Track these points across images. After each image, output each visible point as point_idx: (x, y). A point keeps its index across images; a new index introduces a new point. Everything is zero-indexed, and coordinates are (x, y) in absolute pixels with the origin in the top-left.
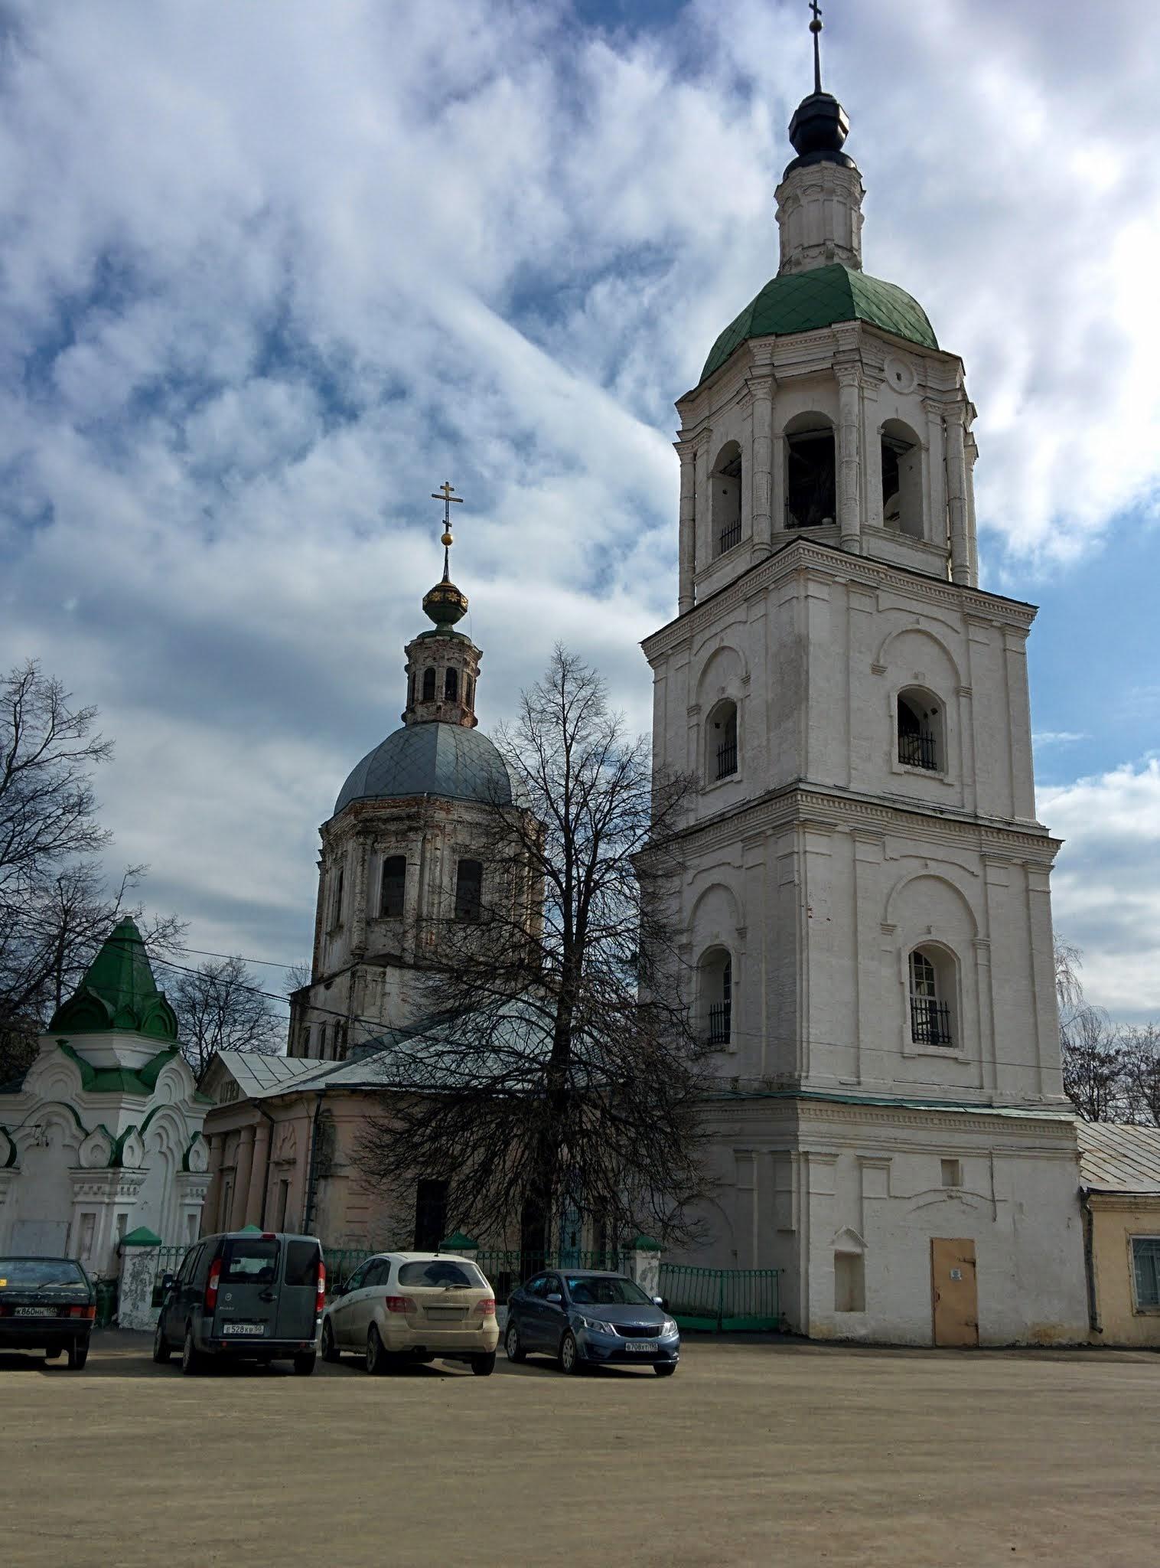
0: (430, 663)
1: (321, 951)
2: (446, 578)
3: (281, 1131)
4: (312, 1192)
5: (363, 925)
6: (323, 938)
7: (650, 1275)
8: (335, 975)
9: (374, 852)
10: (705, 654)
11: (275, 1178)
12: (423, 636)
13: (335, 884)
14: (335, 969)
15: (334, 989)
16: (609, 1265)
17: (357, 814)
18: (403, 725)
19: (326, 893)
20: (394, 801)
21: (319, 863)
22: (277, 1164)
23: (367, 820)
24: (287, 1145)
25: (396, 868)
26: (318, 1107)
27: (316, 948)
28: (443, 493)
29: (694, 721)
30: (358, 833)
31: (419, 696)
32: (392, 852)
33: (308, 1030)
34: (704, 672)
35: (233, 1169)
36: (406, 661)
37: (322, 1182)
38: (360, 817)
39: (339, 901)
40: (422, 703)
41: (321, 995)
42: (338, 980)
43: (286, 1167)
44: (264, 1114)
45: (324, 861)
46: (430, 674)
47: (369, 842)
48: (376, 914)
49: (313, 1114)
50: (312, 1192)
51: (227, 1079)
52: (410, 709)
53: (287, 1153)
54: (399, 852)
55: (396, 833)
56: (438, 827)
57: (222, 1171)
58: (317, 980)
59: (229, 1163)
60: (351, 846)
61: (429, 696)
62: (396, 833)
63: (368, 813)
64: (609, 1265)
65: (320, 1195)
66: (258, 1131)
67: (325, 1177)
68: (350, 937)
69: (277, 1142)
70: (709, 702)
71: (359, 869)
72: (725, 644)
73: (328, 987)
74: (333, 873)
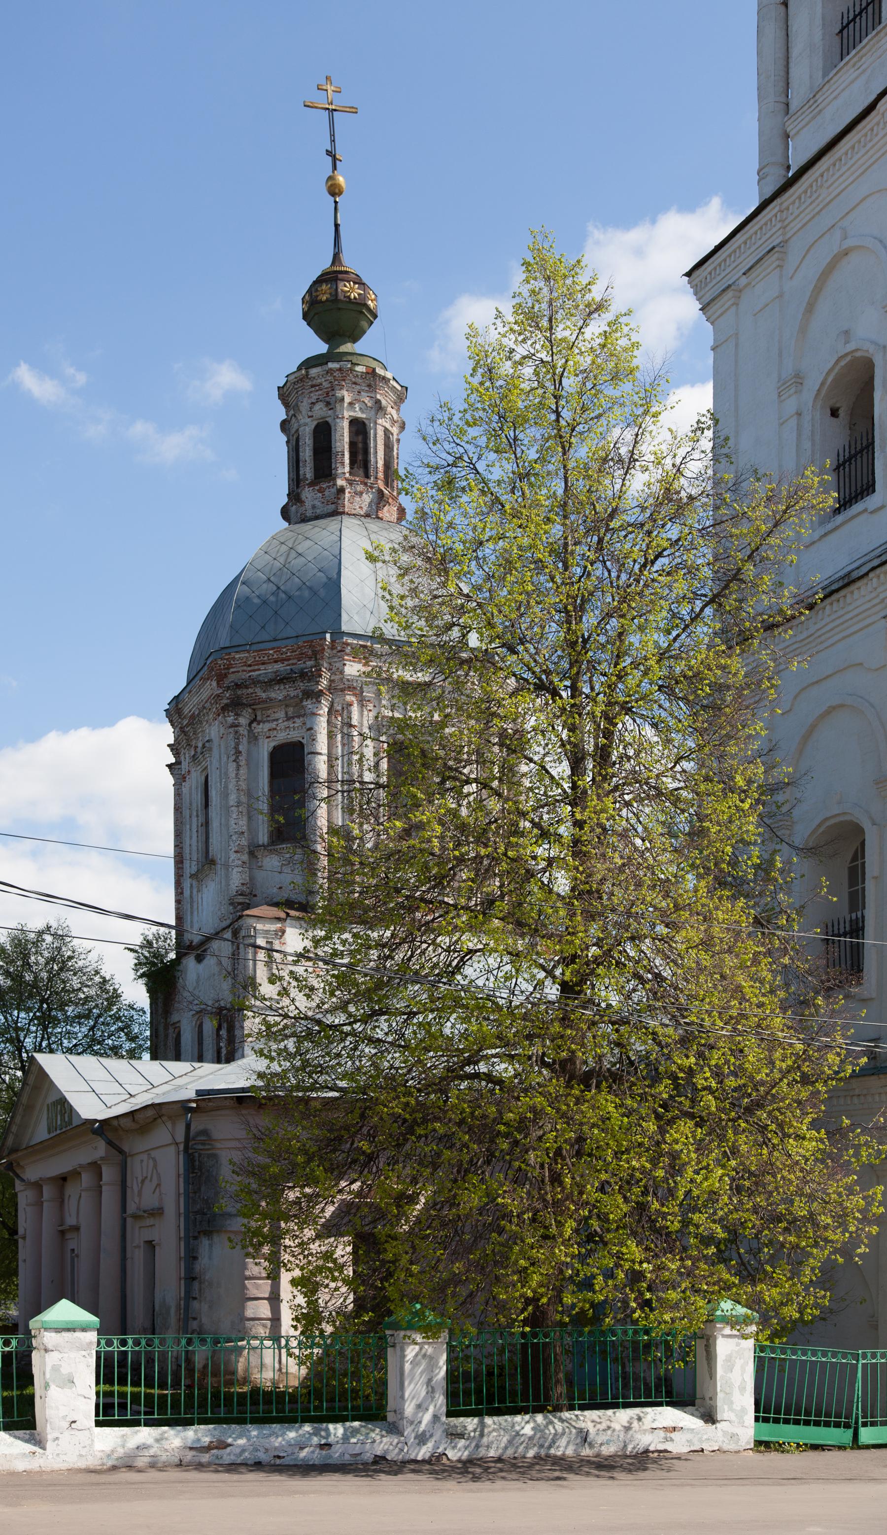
0: (320, 410)
1: (187, 906)
2: (336, 258)
3: (138, 1168)
4: (191, 1257)
5: (245, 858)
6: (187, 884)
7: (739, 1363)
8: (208, 939)
9: (253, 738)
10: (811, 270)
11: (138, 1235)
12: (310, 363)
13: (198, 798)
14: (209, 928)
15: (210, 961)
16: (848, 944)
17: (221, 678)
18: (286, 524)
19: (186, 813)
20: (278, 650)
21: (170, 766)
22: (136, 1217)
23: (238, 686)
24: (149, 1187)
25: (290, 763)
26: (188, 1127)
27: (178, 902)
28: (320, 100)
29: (791, 405)
30: (224, 709)
31: (308, 471)
32: (282, 737)
33: (177, 1026)
34: (810, 308)
35: (77, 1229)
36: (280, 413)
37: (205, 1242)
38: (226, 682)
39: (207, 824)
40: (311, 484)
41: (192, 971)
42: (215, 945)
43: (149, 1221)
44: (110, 1143)
45: (178, 763)
46: (323, 433)
47: (243, 721)
48: (263, 837)
49: (180, 1137)
50: (191, 1257)
51: (51, 1099)
52: (294, 496)
53: (149, 1200)
54: (294, 735)
55: (285, 703)
56: (351, 688)
57: (63, 1233)
58: (184, 948)
59: (71, 1221)
60: (214, 730)
61: (324, 468)
62: (285, 703)
63: (239, 674)
64: (848, 944)
65: (203, 1261)
66: (105, 1170)
67: (208, 1234)
68: (228, 877)
69: (133, 1185)
70: (820, 364)
71: (232, 766)
72: (849, 243)
73: (199, 959)
74: (195, 779)
